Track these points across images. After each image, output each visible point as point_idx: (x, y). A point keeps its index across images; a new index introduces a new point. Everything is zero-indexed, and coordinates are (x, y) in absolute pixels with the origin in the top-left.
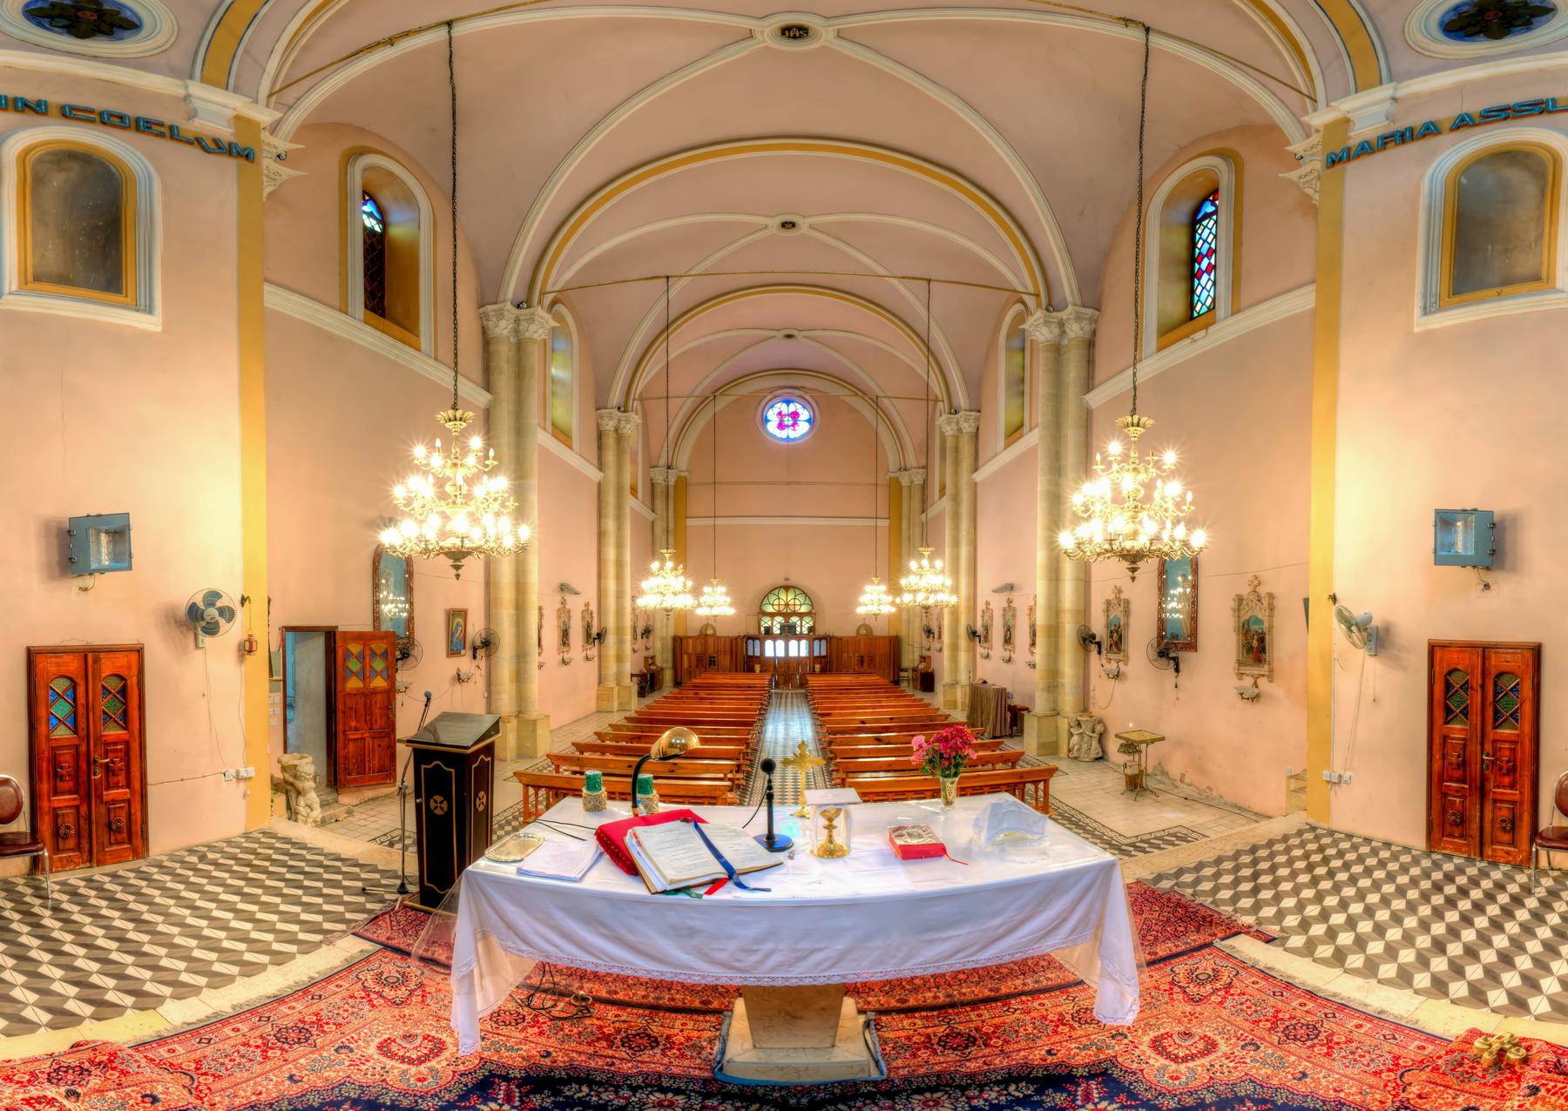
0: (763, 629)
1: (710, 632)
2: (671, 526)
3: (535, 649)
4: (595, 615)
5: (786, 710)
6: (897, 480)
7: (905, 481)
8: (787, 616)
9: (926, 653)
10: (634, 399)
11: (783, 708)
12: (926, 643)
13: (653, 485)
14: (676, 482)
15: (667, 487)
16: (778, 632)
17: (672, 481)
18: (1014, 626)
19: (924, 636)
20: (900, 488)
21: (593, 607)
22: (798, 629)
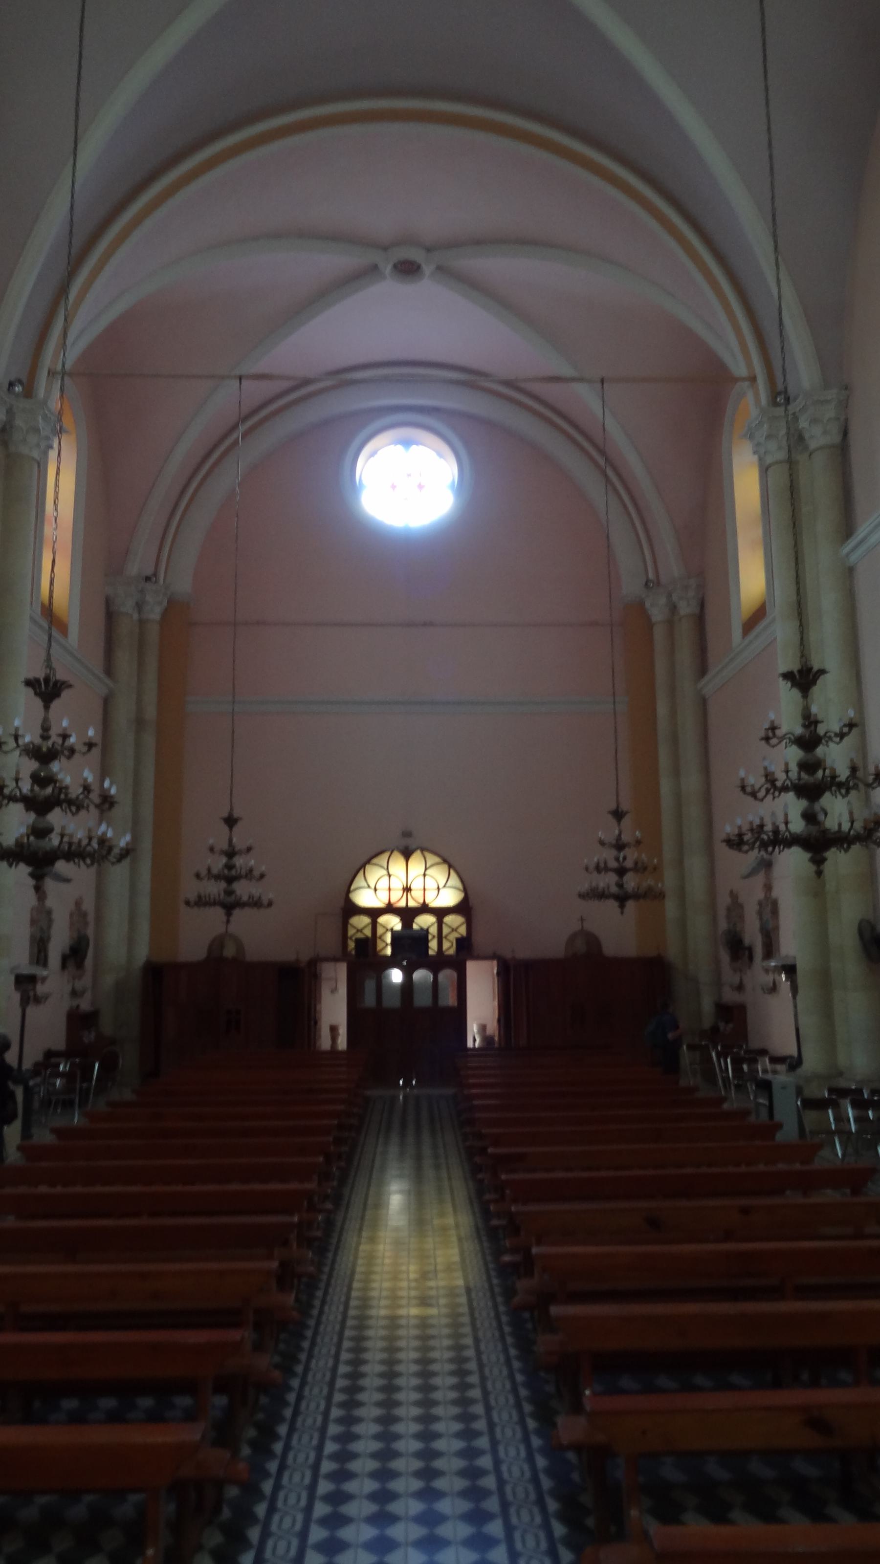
0: (351, 945)
1: (229, 952)
2: (151, 712)
3: (476, 1037)
4: (91, 918)
5: (403, 1135)
6: (639, 609)
7: (657, 613)
8: (407, 914)
9: (730, 996)
10: (753, 379)
11: (395, 1139)
12: (729, 976)
13: (111, 616)
14: (165, 614)
15: (142, 622)
16: (389, 951)
17: (155, 613)
18: (777, 928)
19: (725, 957)
20: (650, 626)
21: (88, 906)
22: (433, 945)
